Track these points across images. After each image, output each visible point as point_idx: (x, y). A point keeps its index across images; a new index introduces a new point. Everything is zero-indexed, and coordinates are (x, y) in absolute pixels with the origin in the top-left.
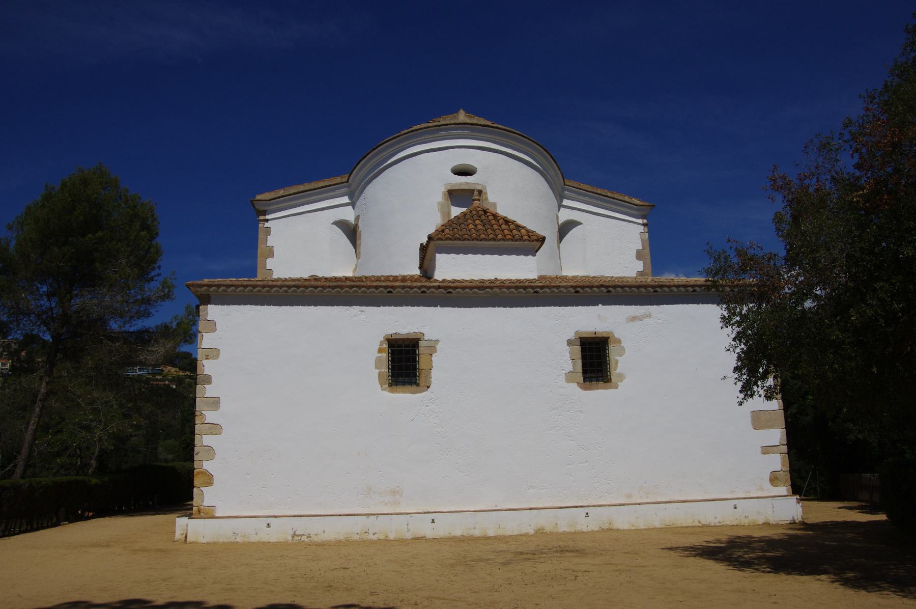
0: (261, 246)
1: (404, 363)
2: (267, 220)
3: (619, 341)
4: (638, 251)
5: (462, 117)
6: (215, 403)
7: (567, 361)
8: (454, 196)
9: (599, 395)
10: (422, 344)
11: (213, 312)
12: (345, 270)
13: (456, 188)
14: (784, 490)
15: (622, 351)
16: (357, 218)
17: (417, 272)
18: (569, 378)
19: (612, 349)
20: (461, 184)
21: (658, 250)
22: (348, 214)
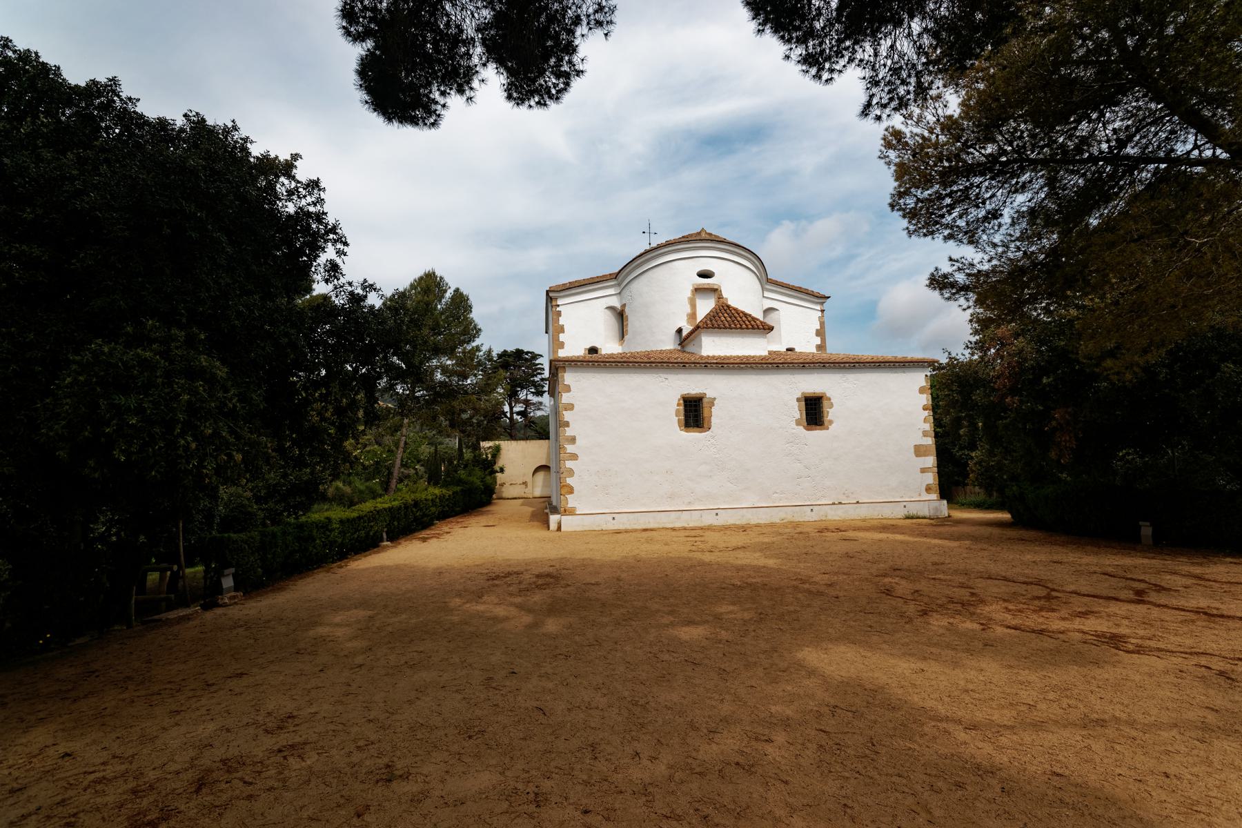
1: (694, 413)
6: (573, 440)
7: (796, 411)
9: (817, 434)
10: (705, 400)
14: (934, 496)
15: (831, 406)
16: (624, 306)
18: (798, 423)
19: (825, 403)
22: (615, 302)
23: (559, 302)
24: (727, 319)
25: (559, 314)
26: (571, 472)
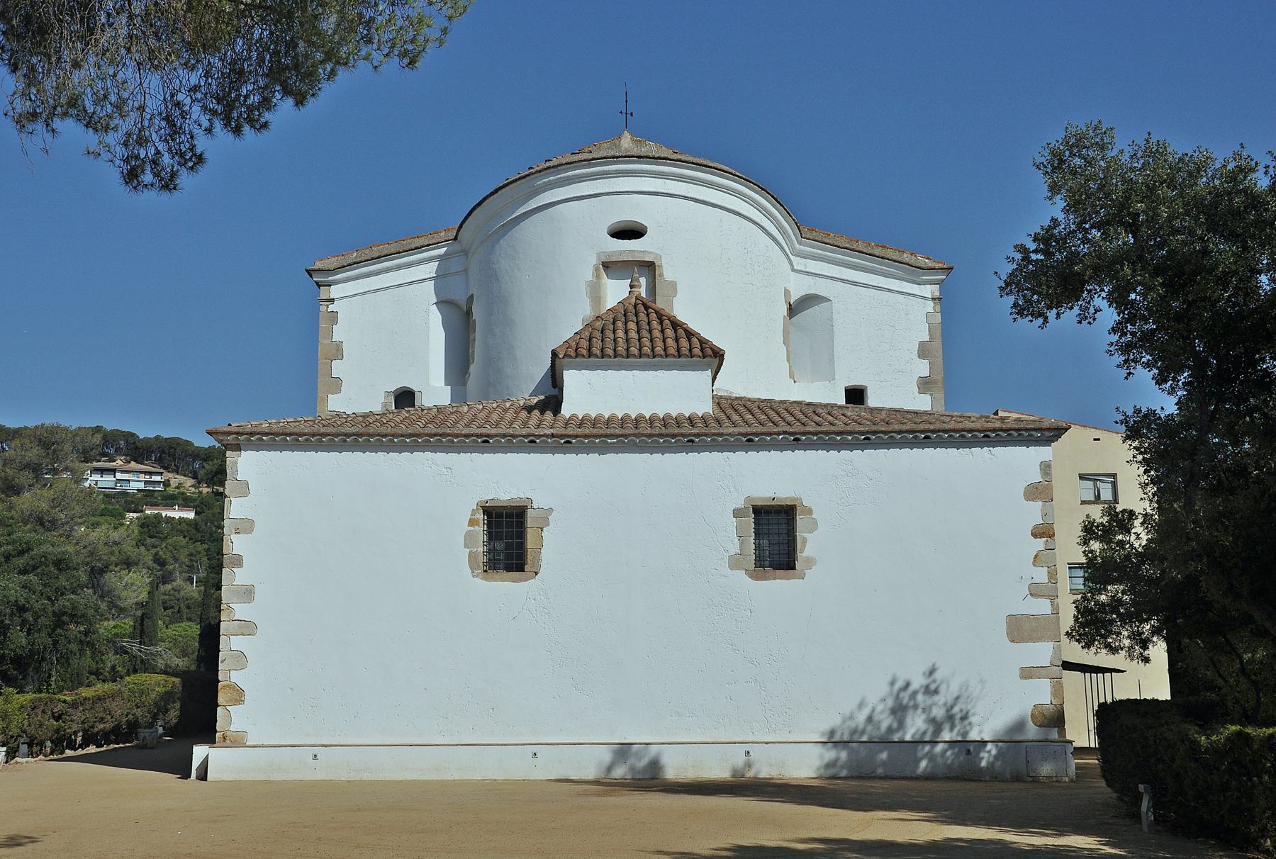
0: (323, 341)
2: (332, 301)
3: (810, 512)
4: (922, 345)
7: (732, 537)
9: (778, 586)
13: (614, 259)
15: (814, 526)
19: (800, 521)
20: (621, 253)
23: (335, 291)
25: (334, 317)
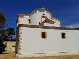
1: (44, 35)
5: (43, 8)
7: (61, 36)
8: (43, 17)
9: (64, 40)
11: (21, 28)
12: (29, 24)
16: (30, 19)
17: (38, 25)
21: (62, 24)
22: (29, 18)
24: (47, 21)
26: (21, 46)
